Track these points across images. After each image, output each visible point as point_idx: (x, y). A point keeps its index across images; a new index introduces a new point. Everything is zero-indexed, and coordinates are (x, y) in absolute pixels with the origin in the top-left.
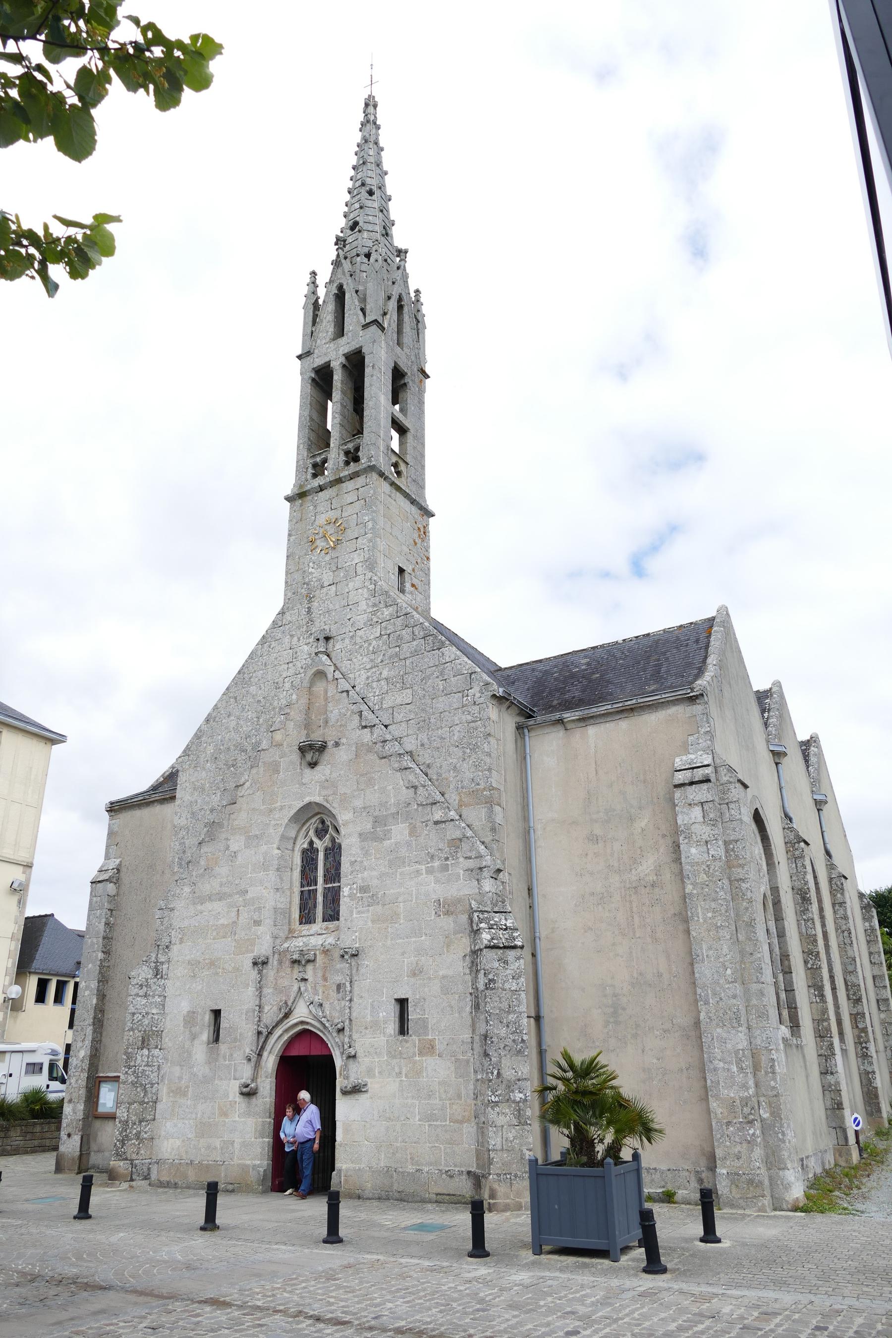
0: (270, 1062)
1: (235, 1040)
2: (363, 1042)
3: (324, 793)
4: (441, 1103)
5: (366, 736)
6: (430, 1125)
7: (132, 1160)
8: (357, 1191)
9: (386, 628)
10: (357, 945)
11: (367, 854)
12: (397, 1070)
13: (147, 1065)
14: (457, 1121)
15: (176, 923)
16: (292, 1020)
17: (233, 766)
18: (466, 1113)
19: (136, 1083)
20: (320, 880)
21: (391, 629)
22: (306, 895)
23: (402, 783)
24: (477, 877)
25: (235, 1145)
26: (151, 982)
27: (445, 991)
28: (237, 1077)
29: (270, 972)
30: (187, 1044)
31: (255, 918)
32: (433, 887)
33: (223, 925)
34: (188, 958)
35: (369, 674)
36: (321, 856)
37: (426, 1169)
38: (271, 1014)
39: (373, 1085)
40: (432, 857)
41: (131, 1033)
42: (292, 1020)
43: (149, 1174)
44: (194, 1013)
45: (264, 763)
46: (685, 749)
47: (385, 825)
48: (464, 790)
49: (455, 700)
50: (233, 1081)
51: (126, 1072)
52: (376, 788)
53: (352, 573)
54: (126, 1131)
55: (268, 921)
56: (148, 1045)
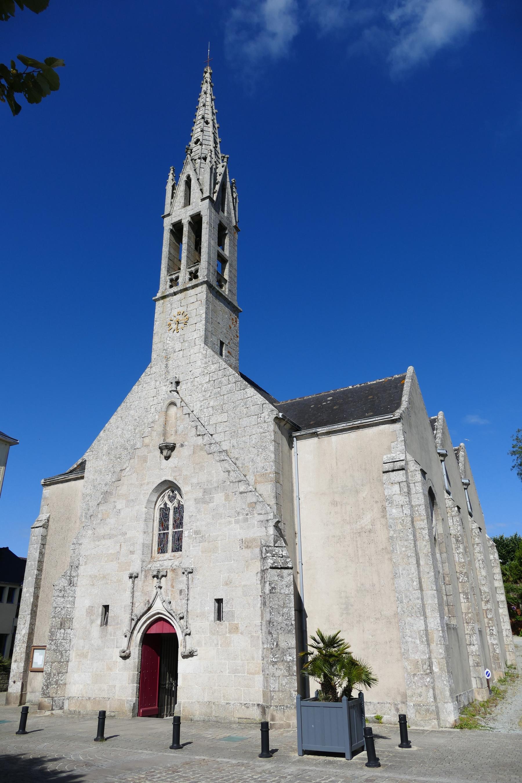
0: (138, 637)
1: (118, 624)
2: (194, 625)
6: (235, 676)
7: (53, 698)
9: (212, 377)
10: (192, 566)
11: (199, 511)
12: (215, 642)
13: (63, 639)
17: (119, 458)
18: (257, 669)
19: (56, 650)
20: (171, 527)
21: (215, 377)
22: (162, 536)
23: (221, 468)
24: (265, 525)
26: (67, 588)
35: (202, 404)
37: (232, 702)
38: (139, 609)
41: (54, 619)
43: (63, 706)
44: (93, 607)
46: (389, 450)
48: (258, 473)
49: (253, 420)
52: (205, 472)
53: (193, 344)
54: (49, 679)
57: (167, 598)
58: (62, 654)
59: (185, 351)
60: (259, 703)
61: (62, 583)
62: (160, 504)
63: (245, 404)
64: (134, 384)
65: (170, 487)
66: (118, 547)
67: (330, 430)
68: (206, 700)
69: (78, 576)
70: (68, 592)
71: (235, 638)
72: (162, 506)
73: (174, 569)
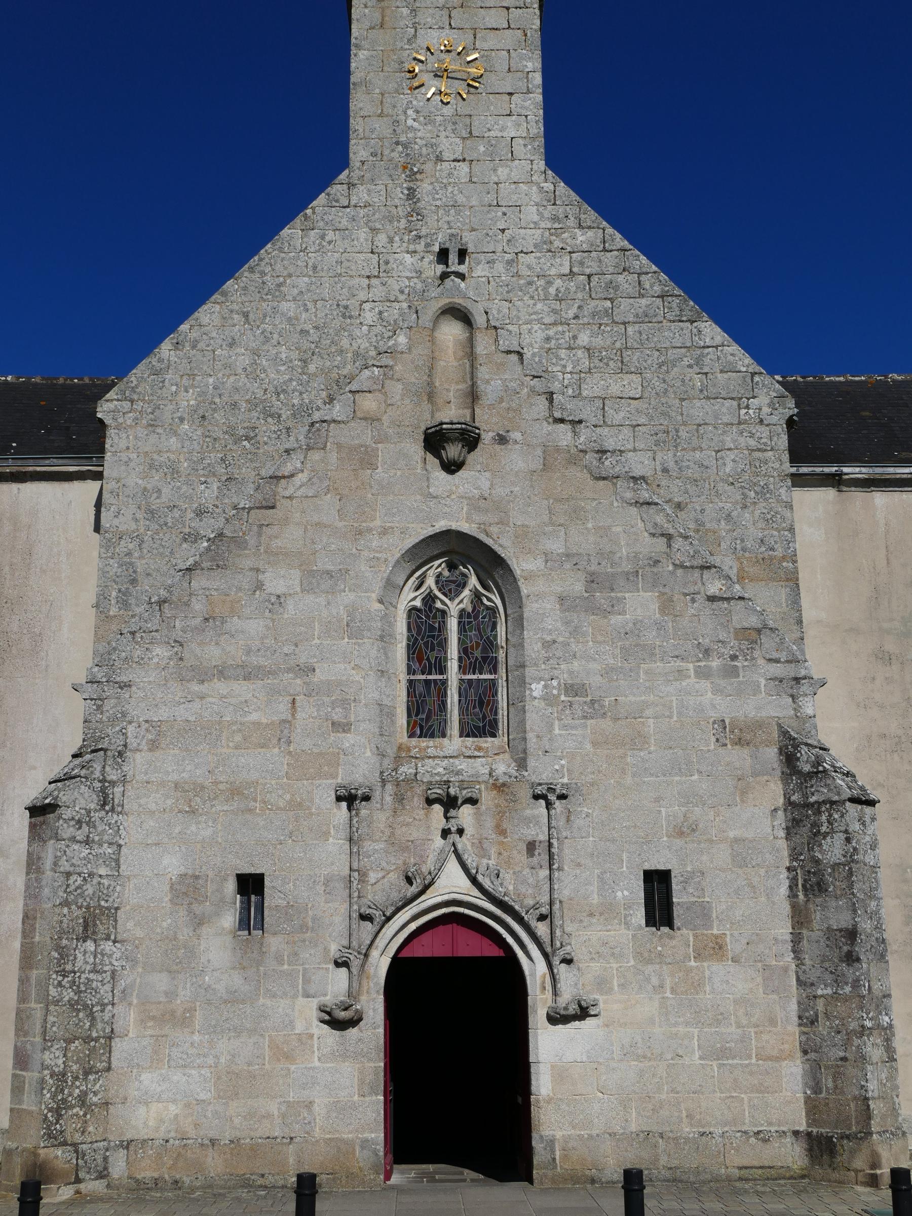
0: (380, 964)
1: (303, 928)
2: (580, 937)
3: (477, 518)
4: (739, 1031)
5: (563, 435)
6: (720, 1066)
7: (75, 1145)
8: (587, 1172)
9: (582, 263)
10: (565, 780)
11: (576, 632)
12: (655, 981)
13: (94, 971)
14: (769, 1058)
15: (137, 710)
16: (430, 899)
17: (248, 438)
18: (786, 1046)
19: (77, 1002)
20: (453, 666)
21: (592, 267)
22: (420, 689)
23: (641, 525)
24: (790, 691)
25: (316, 1108)
26: (96, 816)
27: (740, 861)
28: (312, 992)
29: (376, 815)
30: (185, 933)
31: (335, 718)
32: (711, 700)
33: (257, 724)
34: (175, 777)
35: (551, 333)
36: (453, 625)
37: (718, 1131)
38: (383, 885)
39: (607, 1005)
40: (707, 652)
41: (65, 910)
42: (430, 899)
43: (106, 1168)
44: (197, 877)
45: (339, 446)
47: (612, 590)
48: (747, 555)
49: (724, 410)
50: (301, 1001)
51: (60, 984)
52: (590, 525)
53: (505, 153)
54: (62, 1091)
55: (363, 726)
56: (94, 933)
57: (485, 861)
58: (91, 1016)
59: (476, 167)
60: (797, 1128)
61: (83, 801)
62: (410, 598)
63: (699, 361)
64: (286, 219)
65: (462, 553)
66: (282, 708)
67: (877, 477)
68: (633, 1127)
69: (124, 781)
70: (100, 829)
71: (715, 970)
72: (418, 603)
73: (504, 785)
